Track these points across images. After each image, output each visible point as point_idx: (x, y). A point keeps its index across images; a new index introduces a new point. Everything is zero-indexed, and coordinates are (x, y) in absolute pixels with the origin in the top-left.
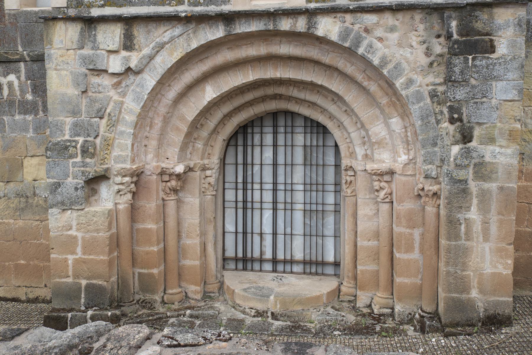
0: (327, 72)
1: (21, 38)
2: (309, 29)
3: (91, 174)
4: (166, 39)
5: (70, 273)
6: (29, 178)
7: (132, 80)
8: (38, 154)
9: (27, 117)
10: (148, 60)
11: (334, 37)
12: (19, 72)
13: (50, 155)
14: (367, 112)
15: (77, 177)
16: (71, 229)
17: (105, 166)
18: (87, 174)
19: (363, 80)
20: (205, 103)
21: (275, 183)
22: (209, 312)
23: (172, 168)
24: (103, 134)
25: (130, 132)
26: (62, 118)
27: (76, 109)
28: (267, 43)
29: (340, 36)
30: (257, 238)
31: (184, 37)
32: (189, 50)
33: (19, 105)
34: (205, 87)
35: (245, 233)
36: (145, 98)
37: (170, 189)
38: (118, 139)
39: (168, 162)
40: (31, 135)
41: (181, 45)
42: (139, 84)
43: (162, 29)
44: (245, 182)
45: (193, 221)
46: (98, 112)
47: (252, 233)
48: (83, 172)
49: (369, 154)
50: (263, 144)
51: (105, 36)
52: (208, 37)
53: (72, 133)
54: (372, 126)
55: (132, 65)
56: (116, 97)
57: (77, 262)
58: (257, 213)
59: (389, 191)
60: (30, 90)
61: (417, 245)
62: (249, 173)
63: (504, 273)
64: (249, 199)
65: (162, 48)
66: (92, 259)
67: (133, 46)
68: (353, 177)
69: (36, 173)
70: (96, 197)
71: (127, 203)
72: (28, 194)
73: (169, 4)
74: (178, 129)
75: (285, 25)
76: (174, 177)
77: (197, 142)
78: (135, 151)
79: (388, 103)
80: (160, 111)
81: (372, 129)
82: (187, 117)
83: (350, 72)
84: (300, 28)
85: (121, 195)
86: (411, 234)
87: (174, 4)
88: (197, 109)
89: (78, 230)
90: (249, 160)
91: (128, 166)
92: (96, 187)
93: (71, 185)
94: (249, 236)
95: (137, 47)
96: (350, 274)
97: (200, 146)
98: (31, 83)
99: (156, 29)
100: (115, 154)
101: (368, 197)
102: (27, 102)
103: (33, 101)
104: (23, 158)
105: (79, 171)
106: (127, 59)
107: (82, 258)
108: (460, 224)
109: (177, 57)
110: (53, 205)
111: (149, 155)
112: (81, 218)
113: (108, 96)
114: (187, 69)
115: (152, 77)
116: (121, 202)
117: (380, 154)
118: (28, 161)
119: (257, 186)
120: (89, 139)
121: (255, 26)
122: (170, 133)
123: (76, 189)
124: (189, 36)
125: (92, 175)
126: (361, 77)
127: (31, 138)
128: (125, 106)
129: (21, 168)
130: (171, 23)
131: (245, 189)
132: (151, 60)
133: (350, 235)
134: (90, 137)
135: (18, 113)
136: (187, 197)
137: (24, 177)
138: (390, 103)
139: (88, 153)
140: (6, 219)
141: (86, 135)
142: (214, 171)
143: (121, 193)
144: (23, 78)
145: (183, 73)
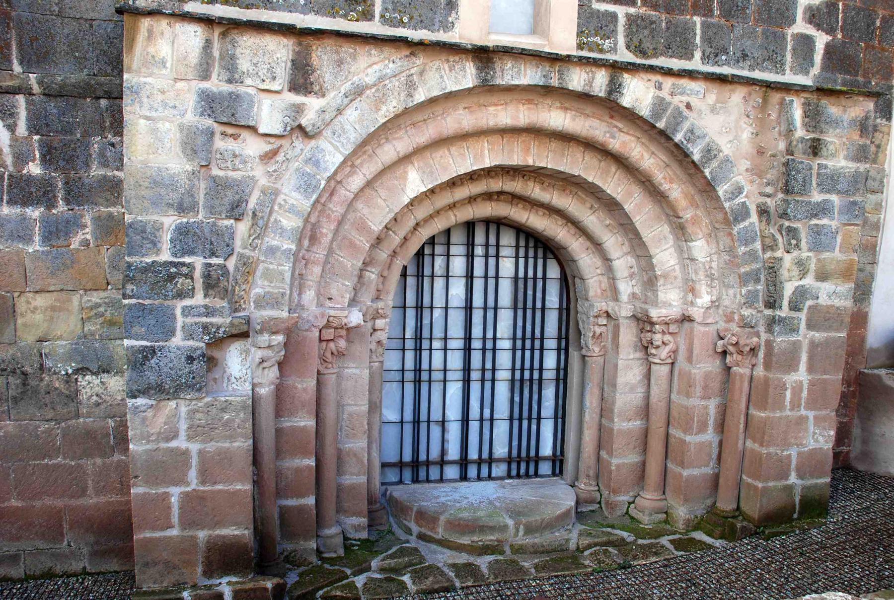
0: (603, 163)
2: (610, 93)
3: (222, 330)
6: (28, 338)
8: (52, 288)
13: (132, 291)
14: (652, 230)
15: (193, 336)
16: (175, 436)
18: (214, 330)
19: (663, 181)
21: (468, 339)
23: (346, 317)
24: (241, 251)
25: (290, 250)
28: (530, 106)
29: (653, 110)
30: (436, 431)
31: (402, 79)
33: (10, 185)
34: (406, 172)
35: (416, 422)
36: (322, 187)
37: (332, 353)
38: (263, 262)
39: (331, 305)
40: (38, 248)
41: (396, 94)
42: (310, 159)
44: (418, 338)
45: (358, 408)
46: (233, 209)
47: (429, 422)
48: (205, 327)
49: (637, 292)
50: (450, 274)
51: (255, 61)
52: (446, 84)
53: (178, 247)
54: (658, 251)
57: (187, 498)
58: (437, 389)
59: (674, 348)
60: (38, 156)
61: (711, 422)
62: (426, 321)
64: (425, 365)
66: (220, 491)
67: (309, 86)
68: (604, 327)
69: (46, 325)
71: (273, 383)
72: (28, 369)
73: (345, 16)
77: (369, 269)
80: (333, 212)
81: (657, 256)
82: (370, 224)
83: (647, 167)
84: (598, 89)
85: (264, 368)
87: (354, 17)
88: (390, 211)
89: (190, 438)
90: (426, 301)
93: (179, 352)
94: (423, 427)
95: (316, 88)
96: (591, 473)
97: (373, 276)
98: (40, 141)
100: (258, 290)
101: (631, 357)
102: (30, 178)
103: (43, 179)
104: (16, 295)
105: (196, 324)
106: (298, 109)
107: (199, 490)
109: (388, 114)
110: (139, 391)
111: (308, 293)
115: (336, 148)
116: (264, 381)
117: (666, 293)
118: (28, 302)
119: (437, 344)
120: (214, 261)
122: (338, 252)
124: (410, 79)
125: (224, 333)
126: (661, 176)
127: (36, 255)
128: (280, 200)
129: (11, 316)
130: (382, 51)
131: (418, 350)
133: (594, 415)
134: (217, 257)
135: (8, 203)
136: (347, 368)
137: (18, 334)
139: (216, 290)
141: (207, 252)
143: (265, 365)
144: (22, 129)
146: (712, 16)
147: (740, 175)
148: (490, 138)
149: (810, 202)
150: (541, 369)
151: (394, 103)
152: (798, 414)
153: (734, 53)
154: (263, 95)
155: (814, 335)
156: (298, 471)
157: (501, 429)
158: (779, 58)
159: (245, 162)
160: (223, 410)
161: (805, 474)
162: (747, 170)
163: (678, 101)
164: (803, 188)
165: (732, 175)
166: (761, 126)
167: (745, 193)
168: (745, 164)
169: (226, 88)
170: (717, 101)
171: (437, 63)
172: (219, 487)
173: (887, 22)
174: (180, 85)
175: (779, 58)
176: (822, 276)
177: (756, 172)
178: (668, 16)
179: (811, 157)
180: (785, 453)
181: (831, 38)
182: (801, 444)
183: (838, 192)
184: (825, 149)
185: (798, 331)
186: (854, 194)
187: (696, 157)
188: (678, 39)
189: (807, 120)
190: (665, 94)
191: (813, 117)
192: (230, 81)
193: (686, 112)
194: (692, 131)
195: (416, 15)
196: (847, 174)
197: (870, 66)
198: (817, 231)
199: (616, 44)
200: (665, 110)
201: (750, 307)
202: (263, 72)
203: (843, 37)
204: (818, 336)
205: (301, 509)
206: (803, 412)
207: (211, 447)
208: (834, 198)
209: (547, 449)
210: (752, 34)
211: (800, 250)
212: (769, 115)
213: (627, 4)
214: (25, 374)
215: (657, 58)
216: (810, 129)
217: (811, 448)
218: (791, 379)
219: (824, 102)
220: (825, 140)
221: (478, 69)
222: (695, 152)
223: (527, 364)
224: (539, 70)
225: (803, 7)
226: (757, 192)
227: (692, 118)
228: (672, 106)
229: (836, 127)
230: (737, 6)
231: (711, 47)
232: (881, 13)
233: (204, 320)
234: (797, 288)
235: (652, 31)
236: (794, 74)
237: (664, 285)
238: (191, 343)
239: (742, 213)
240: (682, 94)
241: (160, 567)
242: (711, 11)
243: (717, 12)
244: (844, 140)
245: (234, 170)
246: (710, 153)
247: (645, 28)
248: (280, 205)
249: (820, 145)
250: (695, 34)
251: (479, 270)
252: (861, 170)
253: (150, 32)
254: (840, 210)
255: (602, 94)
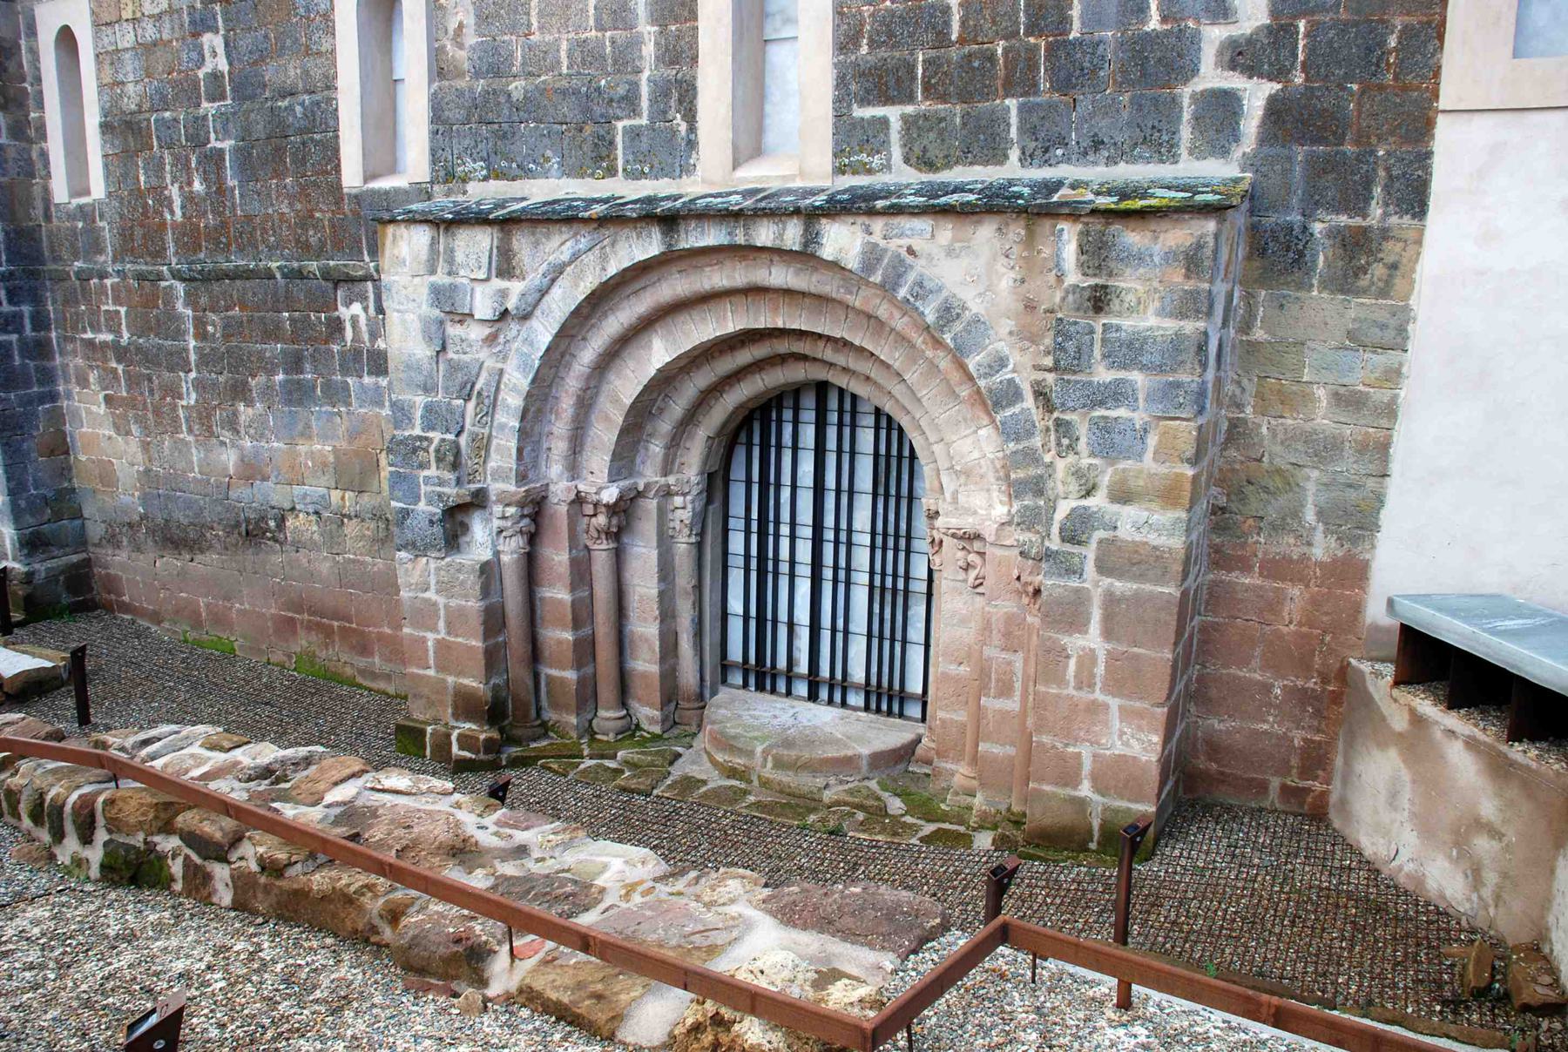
1: (367, 238)
2: (806, 245)
4: (565, 257)
5: (432, 662)
7: (514, 332)
9: (380, 379)
10: (538, 295)
11: (852, 262)
12: (366, 298)
14: (946, 408)
17: (473, 487)
20: (653, 372)
22: (282, 753)
26: (410, 397)
27: (429, 382)
32: (604, 279)
36: (536, 366)
43: (556, 240)
48: (440, 495)
55: (511, 304)
56: (490, 363)
63: (1144, 759)
65: (561, 273)
70: (467, 539)
74: (607, 419)
75: (764, 234)
76: (603, 509)
78: (527, 459)
79: (970, 396)
86: (1009, 663)
91: (512, 488)
92: (466, 520)
95: (518, 272)
97: (658, 449)
99: (548, 236)
106: (504, 294)
108: (1068, 657)
112: (442, 573)
113: (477, 360)
114: (611, 309)
117: (968, 496)
119: (785, 530)
121: (712, 236)
123: (431, 522)
132: (543, 295)
138: (976, 397)
140: (361, 554)
142: (689, 498)
143: (504, 534)
145: (605, 315)
146: (1036, 93)
147: (1001, 340)
148: (732, 299)
149: (1090, 383)
150: (907, 578)
151: (590, 279)
152: (1091, 697)
153: (1078, 143)
154: (475, 285)
155: (1112, 584)
156: (560, 642)
157: (858, 648)
158: (1165, 138)
159: (471, 346)
160: (459, 571)
161: (1107, 788)
162: (1011, 333)
163: (896, 245)
164: (1075, 362)
165: (987, 341)
166: (1030, 267)
167: (1011, 367)
168: (1007, 325)
169: (447, 280)
170: (955, 239)
171: (626, 230)
172: (460, 640)
173: (1417, 36)
174: (417, 280)
175: (1165, 138)
176: (1122, 495)
177: (1027, 336)
178: (965, 106)
179: (1091, 313)
180: (1071, 749)
181: (1279, 86)
182: (1098, 743)
183: (1143, 368)
184: (1117, 301)
185: (1081, 575)
186: (1173, 371)
187: (930, 318)
188: (982, 137)
189: (1084, 257)
190: (877, 238)
191: (1096, 254)
192: (449, 274)
193: (909, 259)
194: (921, 285)
195: (656, 163)
196: (1159, 339)
197: (1372, 123)
198: (1104, 428)
199: (889, 160)
200: (879, 260)
201: (1029, 529)
202: (472, 262)
203: (1307, 80)
204: (1120, 586)
205: (562, 681)
206: (1098, 695)
207: (453, 603)
208: (1137, 377)
209: (915, 686)
210: (1111, 108)
211: (1076, 453)
212: (1039, 252)
213: (901, 102)
214: (387, 520)
215: (951, 168)
216: (1090, 272)
217: (1117, 752)
218: (1076, 643)
219: (1116, 227)
220: (1117, 287)
221: (663, 233)
222: (926, 312)
223: (889, 570)
224: (723, 227)
225: (1217, 43)
226: (1030, 364)
227: (919, 267)
228: (890, 254)
229: (1139, 265)
230: (1082, 70)
231: (1037, 140)
232: (1398, 22)
233: (438, 489)
234: (1073, 510)
235: (941, 132)
236: (1197, 159)
237: (966, 485)
238: (431, 508)
239: (1011, 394)
240: (901, 235)
241: (424, 700)
242: (1035, 85)
243: (1044, 85)
244: (1156, 284)
245: (465, 353)
246: (949, 313)
247: (931, 129)
248: (506, 385)
249: (1107, 294)
250: (1009, 125)
251: (832, 444)
252: (1187, 332)
253: (394, 236)
254: (1148, 395)
255: (796, 248)
